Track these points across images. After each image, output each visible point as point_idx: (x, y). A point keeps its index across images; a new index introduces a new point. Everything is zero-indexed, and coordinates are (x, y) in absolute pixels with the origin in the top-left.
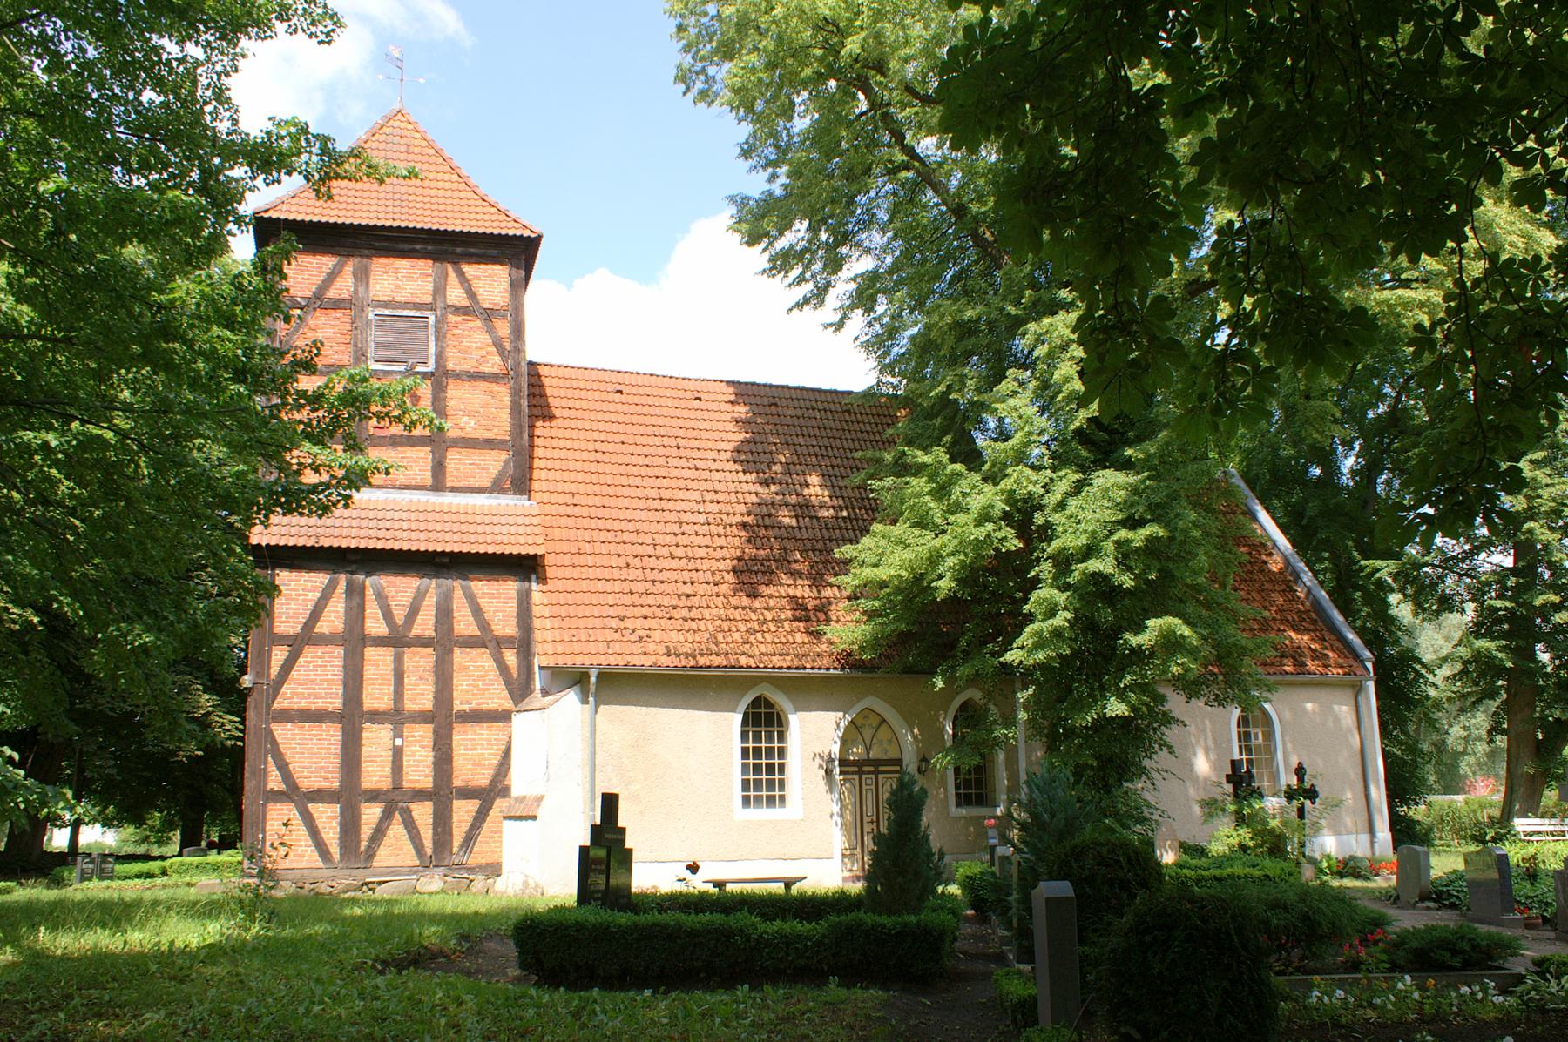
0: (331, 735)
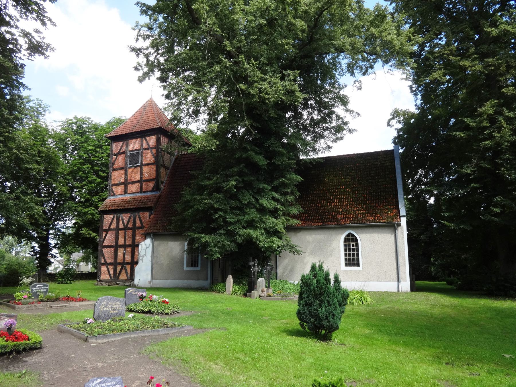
0: (112, 250)
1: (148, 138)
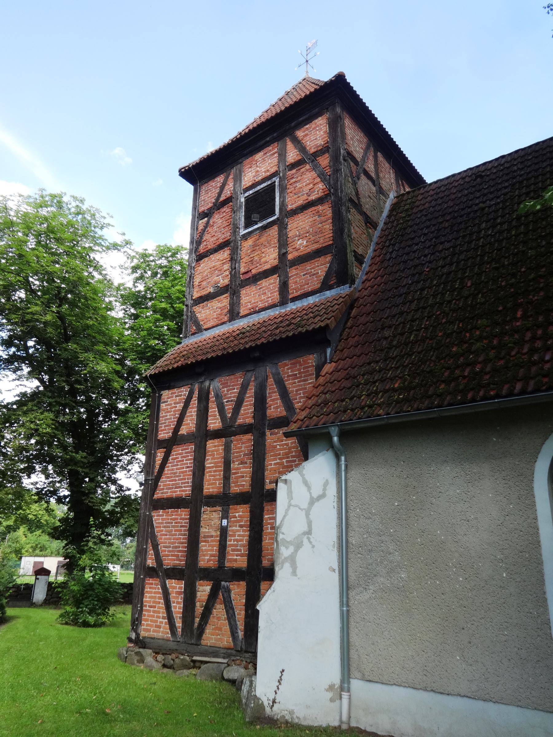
0: (183, 515)
1: (300, 134)
